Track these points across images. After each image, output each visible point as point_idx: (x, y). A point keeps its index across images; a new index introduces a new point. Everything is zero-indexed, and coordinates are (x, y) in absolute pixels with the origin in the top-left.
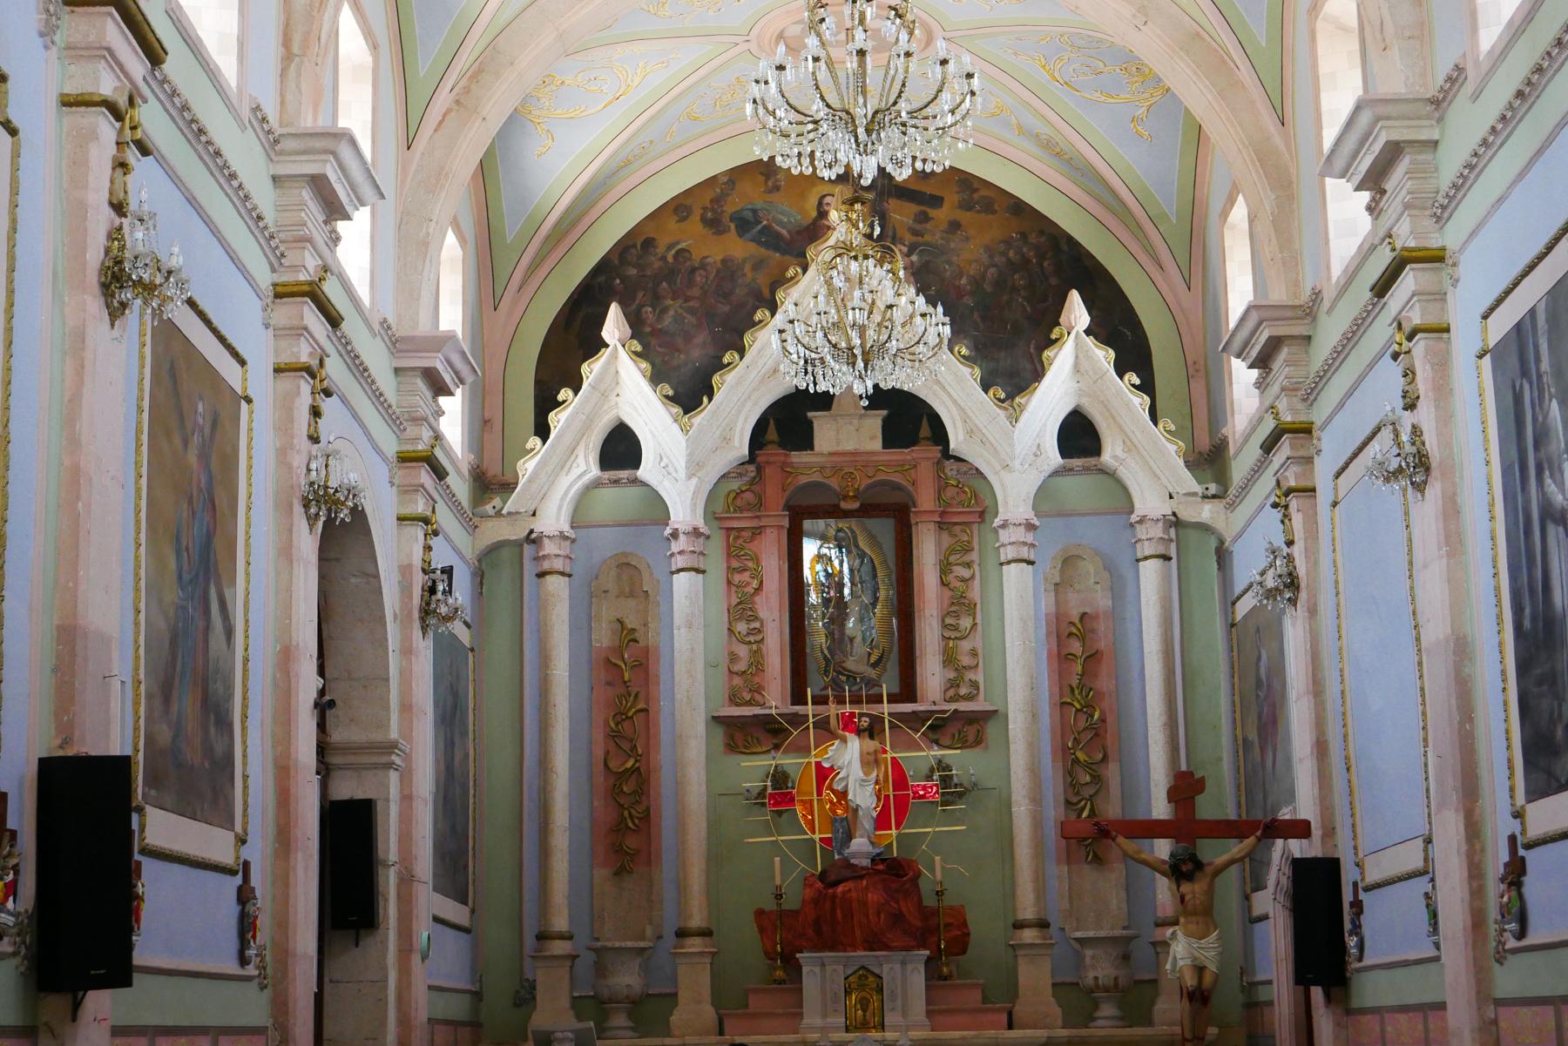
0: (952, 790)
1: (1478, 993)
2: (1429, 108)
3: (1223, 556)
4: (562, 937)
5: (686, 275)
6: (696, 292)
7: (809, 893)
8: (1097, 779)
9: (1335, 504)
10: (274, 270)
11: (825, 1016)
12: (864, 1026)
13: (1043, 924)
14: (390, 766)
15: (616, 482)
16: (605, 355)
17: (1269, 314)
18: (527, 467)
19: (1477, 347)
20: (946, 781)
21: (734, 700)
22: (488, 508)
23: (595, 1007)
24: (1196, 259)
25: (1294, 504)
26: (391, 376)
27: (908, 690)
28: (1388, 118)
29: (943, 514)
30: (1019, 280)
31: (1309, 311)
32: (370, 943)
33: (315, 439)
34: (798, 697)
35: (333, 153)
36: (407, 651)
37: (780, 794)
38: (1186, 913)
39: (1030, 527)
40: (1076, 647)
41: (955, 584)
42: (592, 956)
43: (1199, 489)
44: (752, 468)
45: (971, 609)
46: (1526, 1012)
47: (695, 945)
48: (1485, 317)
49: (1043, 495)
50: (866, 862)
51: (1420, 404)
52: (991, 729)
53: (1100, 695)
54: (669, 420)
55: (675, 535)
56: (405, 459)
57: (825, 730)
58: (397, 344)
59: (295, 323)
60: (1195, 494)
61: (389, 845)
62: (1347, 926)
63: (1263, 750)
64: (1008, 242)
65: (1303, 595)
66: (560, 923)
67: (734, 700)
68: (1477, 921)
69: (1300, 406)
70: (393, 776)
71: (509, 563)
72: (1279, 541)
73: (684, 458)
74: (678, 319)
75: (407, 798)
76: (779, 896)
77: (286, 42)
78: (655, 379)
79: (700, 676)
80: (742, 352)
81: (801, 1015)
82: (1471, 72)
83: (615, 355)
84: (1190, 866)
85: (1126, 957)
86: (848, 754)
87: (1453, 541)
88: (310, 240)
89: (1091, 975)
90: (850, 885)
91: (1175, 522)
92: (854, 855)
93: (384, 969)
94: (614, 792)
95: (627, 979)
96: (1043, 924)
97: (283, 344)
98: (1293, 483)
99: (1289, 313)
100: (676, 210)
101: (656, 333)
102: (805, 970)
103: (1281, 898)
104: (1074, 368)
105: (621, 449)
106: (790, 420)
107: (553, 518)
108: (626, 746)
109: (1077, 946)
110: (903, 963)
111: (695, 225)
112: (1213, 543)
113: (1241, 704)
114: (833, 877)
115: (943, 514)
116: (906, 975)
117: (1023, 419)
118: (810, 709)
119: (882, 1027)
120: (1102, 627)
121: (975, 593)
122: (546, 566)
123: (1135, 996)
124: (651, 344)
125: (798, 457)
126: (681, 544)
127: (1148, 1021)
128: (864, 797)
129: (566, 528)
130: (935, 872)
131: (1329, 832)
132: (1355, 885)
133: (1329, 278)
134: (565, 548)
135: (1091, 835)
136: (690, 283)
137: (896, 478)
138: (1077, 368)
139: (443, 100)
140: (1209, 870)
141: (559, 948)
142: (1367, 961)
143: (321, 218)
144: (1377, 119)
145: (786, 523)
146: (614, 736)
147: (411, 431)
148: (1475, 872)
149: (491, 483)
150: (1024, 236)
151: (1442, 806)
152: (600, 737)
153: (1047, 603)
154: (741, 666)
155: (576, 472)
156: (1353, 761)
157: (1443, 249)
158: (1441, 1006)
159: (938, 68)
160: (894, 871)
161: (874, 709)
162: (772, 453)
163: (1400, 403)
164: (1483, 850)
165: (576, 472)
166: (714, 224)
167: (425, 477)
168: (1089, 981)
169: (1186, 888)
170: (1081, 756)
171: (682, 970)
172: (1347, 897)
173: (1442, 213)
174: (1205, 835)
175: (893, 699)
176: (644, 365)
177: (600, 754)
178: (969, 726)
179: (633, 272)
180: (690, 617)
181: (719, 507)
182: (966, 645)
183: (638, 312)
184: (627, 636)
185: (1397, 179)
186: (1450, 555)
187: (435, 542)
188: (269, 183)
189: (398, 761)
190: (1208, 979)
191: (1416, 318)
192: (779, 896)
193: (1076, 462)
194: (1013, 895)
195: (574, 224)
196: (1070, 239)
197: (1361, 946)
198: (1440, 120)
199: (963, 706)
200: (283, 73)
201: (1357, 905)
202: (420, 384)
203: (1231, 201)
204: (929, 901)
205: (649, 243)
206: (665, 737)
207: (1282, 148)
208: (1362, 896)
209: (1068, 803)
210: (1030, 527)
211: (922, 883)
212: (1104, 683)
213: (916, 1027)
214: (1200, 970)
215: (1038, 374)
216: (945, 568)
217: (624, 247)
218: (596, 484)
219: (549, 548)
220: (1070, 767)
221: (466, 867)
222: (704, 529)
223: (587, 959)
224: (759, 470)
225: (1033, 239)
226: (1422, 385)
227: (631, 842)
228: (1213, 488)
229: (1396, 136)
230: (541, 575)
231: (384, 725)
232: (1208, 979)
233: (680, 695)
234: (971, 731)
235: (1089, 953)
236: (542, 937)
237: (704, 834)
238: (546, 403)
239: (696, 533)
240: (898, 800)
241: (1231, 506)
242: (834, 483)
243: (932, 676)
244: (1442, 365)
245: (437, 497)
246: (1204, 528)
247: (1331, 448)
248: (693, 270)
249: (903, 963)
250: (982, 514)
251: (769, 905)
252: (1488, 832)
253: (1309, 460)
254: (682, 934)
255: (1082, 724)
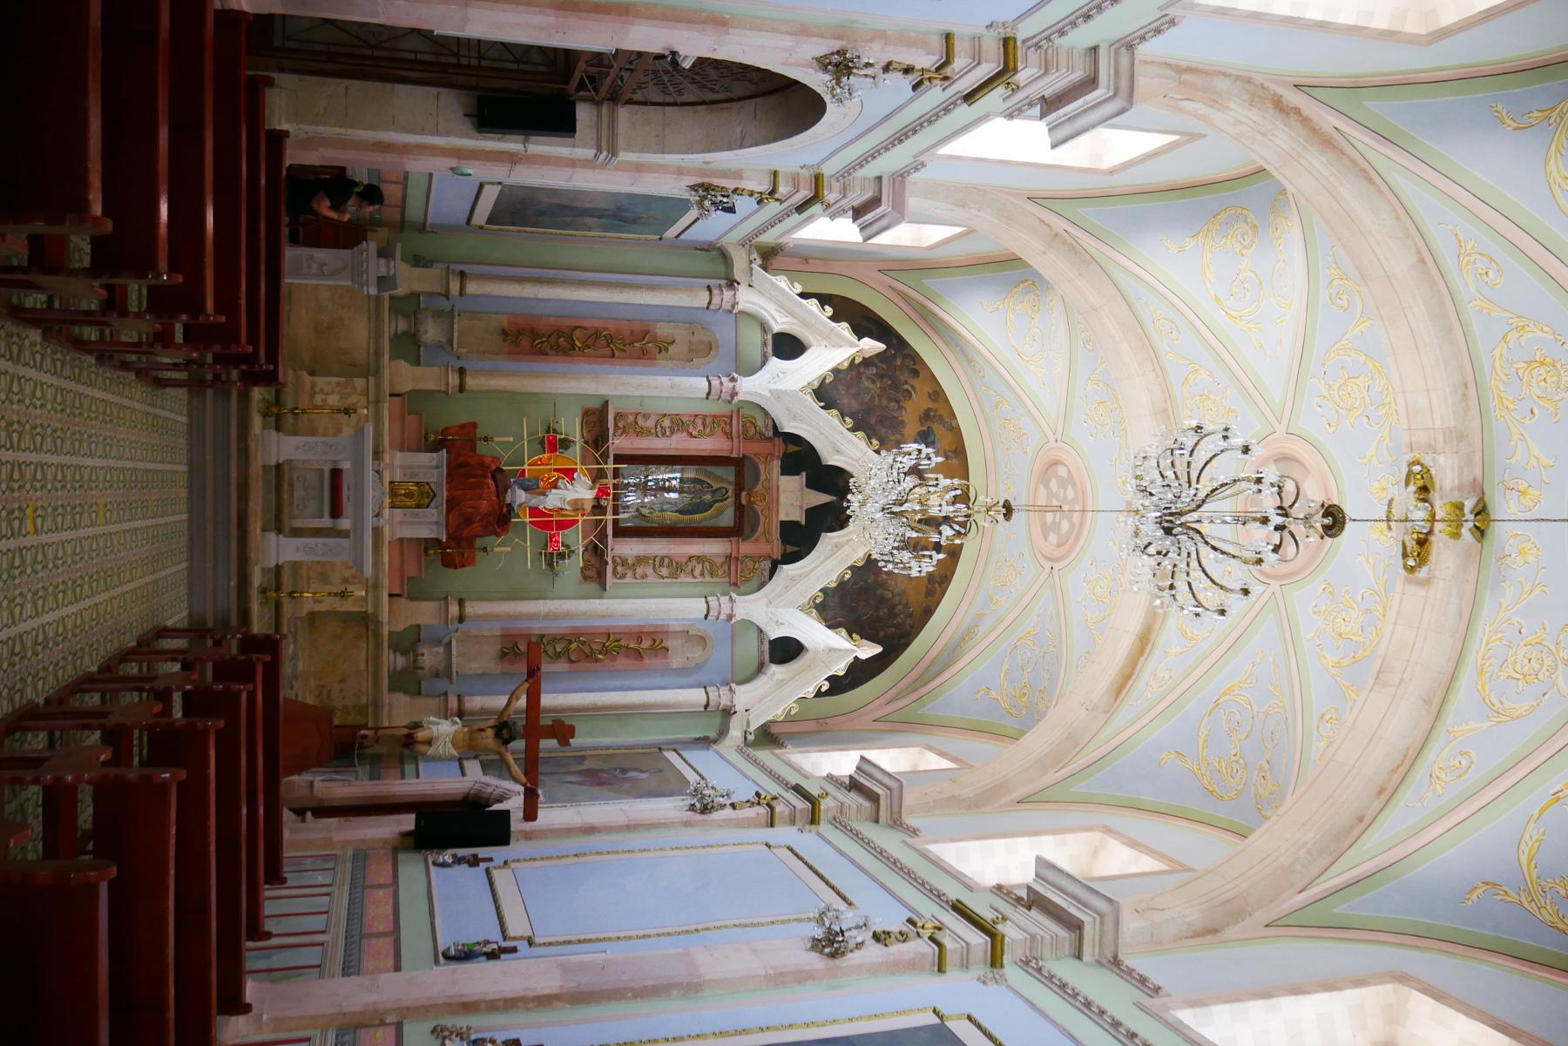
0: (553, 559)
1: (408, 1009)
2: (1109, 955)
3: (705, 742)
4: (462, 288)
5: (893, 389)
6: (884, 403)
7: (488, 461)
8: (558, 656)
9: (768, 845)
10: (1024, 42)
11: (401, 467)
12: (393, 494)
13: (461, 619)
14: (599, 150)
15: (765, 344)
16: (854, 338)
17: (896, 793)
18: (782, 282)
19: (944, 1011)
20: (562, 556)
21: (619, 416)
22: (755, 255)
23: (409, 306)
24: (900, 725)
25: (762, 810)
26: (877, 174)
27: (621, 532)
28: (1102, 923)
29: (737, 559)
30: (883, 612)
31: (896, 823)
32: (467, 125)
33: (887, 68)
34: (619, 459)
35: (1115, 95)
36: (681, 171)
37: (554, 443)
38: (471, 732)
39: (730, 617)
40: (646, 644)
41: (691, 565)
42: (448, 309)
43: (753, 728)
44: (771, 434)
45: (674, 575)
46: (389, 909)
47: (454, 380)
48: (970, 1018)
49: (748, 624)
50: (508, 500)
51: (880, 946)
52: (593, 587)
53: (614, 659)
54: (810, 379)
55: (733, 380)
56: (818, 179)
57: (598, 476)
58: (901, 177)
59: (983, 55)
60: (748, 725)
61: (542, 146)
62: (461, 852)
63: (579, 773)
64: (906, 606)
65: (698, 817)
66: (472, 288)
67: (619, 416)
68: (468, 1007)
69: (830, 815)
70: (589, 153)
71: (717, 265)
72: (734, 799)
73: (784, 389)
74: (868, 390)
75: (573, 163)
76: (486, 439)
77: (1190, 70)
78: (836, 371)
79: (636, 393)
80: (853, 430)
81: (402, 450)
82: (1157, 1001)
83: (852, 345)
84: (506, 736)
85: (437, 675)
86: (582, 491)
87: (779, 979)
88: (1046, 72)
89: (426, 651)
90: (493, 488)
91: (728, 713)
92: (514, 492)
93: (447, 134)
94: (558, 332)
95: (431, 332)
96: (461, 619)
97: (967, 44)
98: (778, 809)
99: (895, 809)
100: (935, 392)
101: (859, 374)
102: (434, 455)
103: (478, 786)
104: (834, 648)
105: (789, 346)
106: (799, 456)
107: (747, 299)
108: (589, 342)
109: (445, 641)
110: (437, 523)
111: (927, 404)
112: (712, 735)
113: (607, 754)
114: (498, 476)
115: (737, 559)
116: (428, 525)
117: (802, 615)
118: (611, 466)
119: (393, 507)
120: (659, 661)
121: (684, 578)
122: (716, 292)
123: (409, 682)
124: (857, 369)
125: (776, 465)
126: (727, 384)
127: (392, 689)
128: (553, 500)
129: (740, 307)
130: (500, 548)
131: (528, 836)
132: (491, 860)
133: (929, 842)
134: (727, 306)
135: (529, 655)
136: (890, 400)
137: (761, 529)
138: (832, 650)
139: (1059, 224)
140: (502, 749)
141: (455, 286)
142: (433, 869)
143: (1047, 94)
144: (1101, 915)
145: (734, 455)
146: (597, 334)
147: (836, 186)
148: (509, 1004)
149: (769, 256)
150: (911, 615)
151: (565, 969)
152: (597, 324)
153: (675, 626)
154: (640, 421)
155: (777, 315)
156: (583, 859)
157: (1002, 966)
158: (397, 968)
159: (1238, 586)
160: (502, 519)
161: (610, 509)
162: (780, 448)
163: (879, 929)
164: (528, 1009)
165: (777, 315)
166: (926, 416)
167: (804, 193)
168: (421, 650)
169: (490, 732)
170: (574, 646)
171: (436, 370)
172: (482, 852)
173: (1029, 963)
174: (532, 742)
175: (615, 522)
176: (846, 364)
177: (585, 324)
178: (597, 571)
179: (899, 362)
180: (670, 389)
181: (746, 411)
182: (650, 571)
183: (873, 364)
184: (663, 346)
185: (854, 799)
186: (767, 977)
187: (753, 201)
188: (1093, 44)
189: (602, 157)
190: (422, 748)
191: (779, 808)
192: (486, 439)
193: (766, 647)
194: (482, 599)
195: (932, 326)
196: (908, 645)
197: (444, 865)
198: (1099, 963)
199: (609, 568)
200: (1168, 65)
201: (474, 862)
202: (869, 195)
203: (942, 754)
204: (480, 542)
205: (916, 373)
206: (596, 367)
207: (1002, 802)
208: (483, 865)
209: (543, 636)
210: (730, 617)
211: (492, 538)
212: (621, 662)
213: (392, 531)
214: (429, 742)
215: (832, 626)
216: (700, 559)
217: (914, 357)
218: (764, 327)
219: (728, 294)
220: (567, 639)
221: (513, 224)
222: (736, 399)
223: (447, 306)
224: (770, 439)
225: (909, 621)
226: (897, 949)
227: (525, 342)
228: (751, 738)
229: (1087, 930)
230: (709, 288)
231: (629, 148)
232: (422, 748)
233: (625, 378)
234: (592, 573)
235: (441, 649)
236: (462, 275)
237: (530, 390)
238: (823, 299)
239: (734, 394)
240: (550, 523)
241: (740, 750)
242: (759, 487)
243: (630, 548)
244: (913, 966)
245: (785, 205)
246: (723, 732)
247: (805, 840)
248: (898, 402)
249: (437, 523)
250: (735, 584)
251: (480, 433)
252: (544, 1016)
253: (792, 822)
254: (462, 371)
255: (595, 647)
